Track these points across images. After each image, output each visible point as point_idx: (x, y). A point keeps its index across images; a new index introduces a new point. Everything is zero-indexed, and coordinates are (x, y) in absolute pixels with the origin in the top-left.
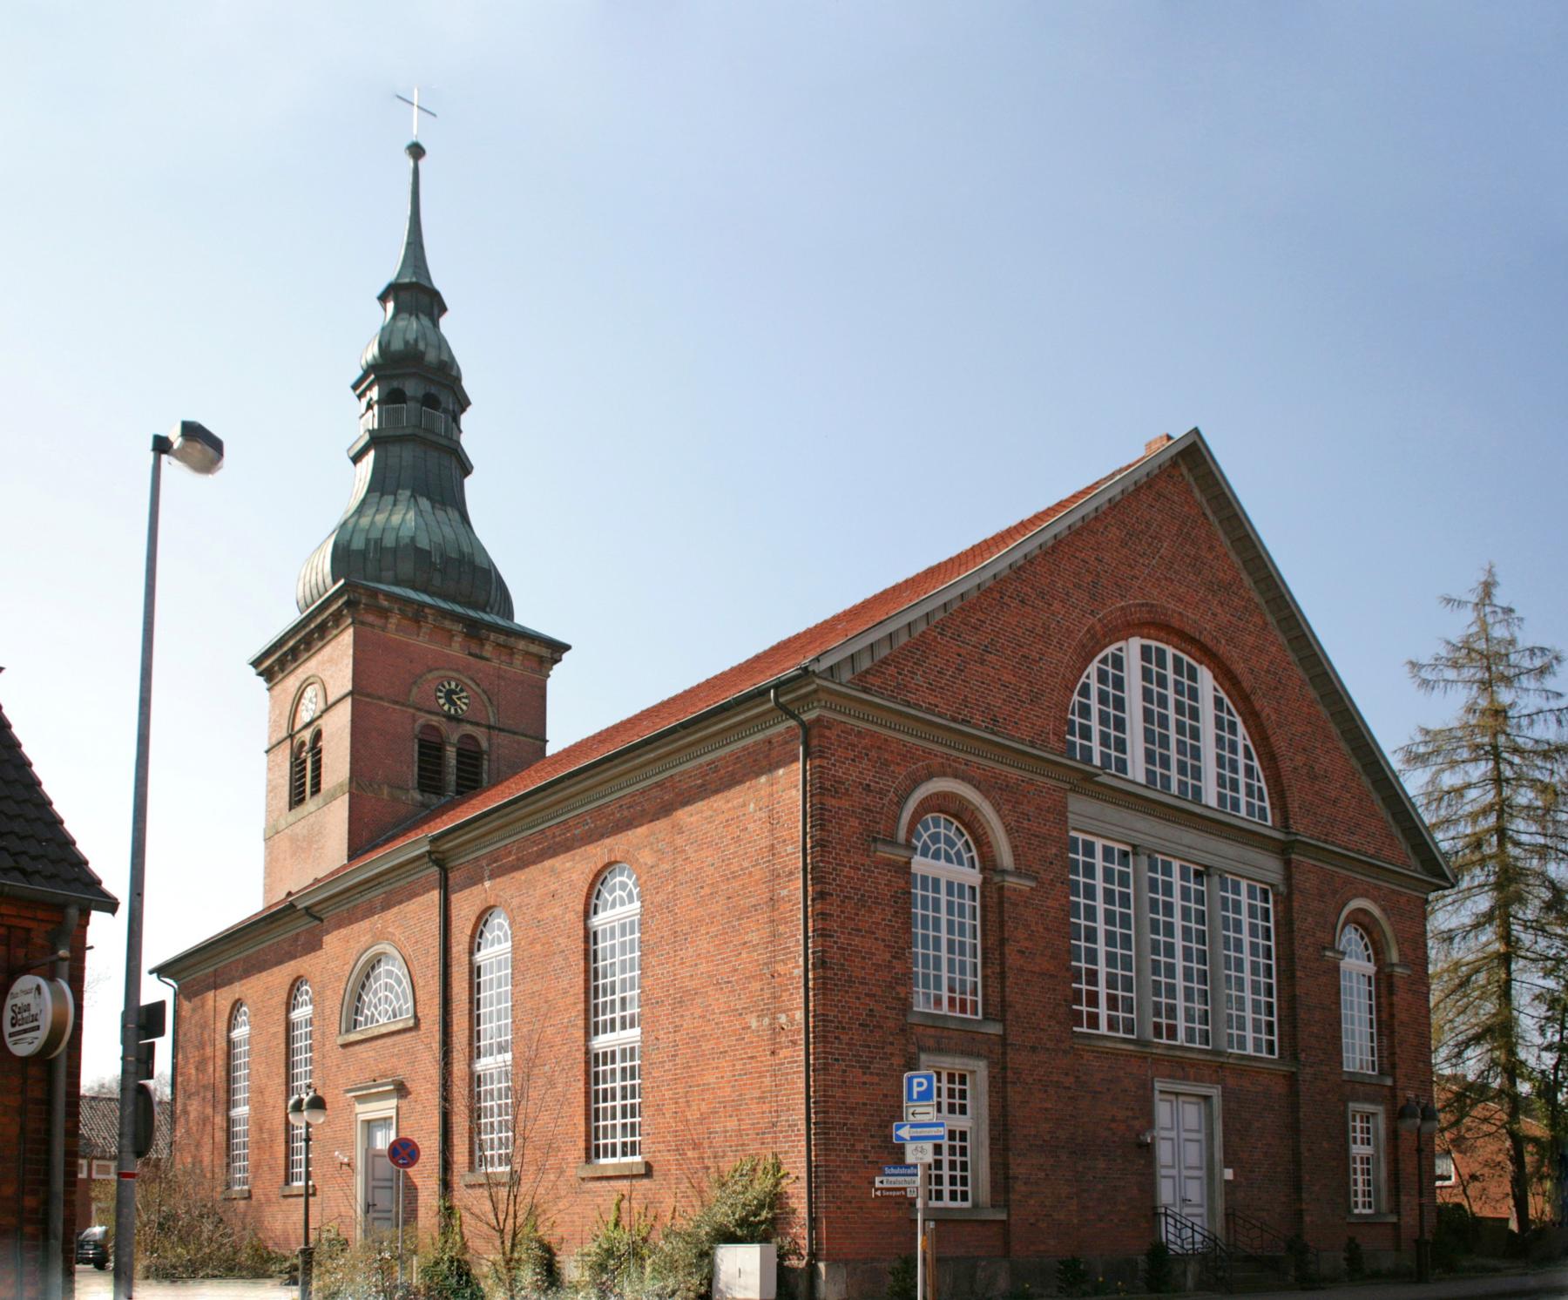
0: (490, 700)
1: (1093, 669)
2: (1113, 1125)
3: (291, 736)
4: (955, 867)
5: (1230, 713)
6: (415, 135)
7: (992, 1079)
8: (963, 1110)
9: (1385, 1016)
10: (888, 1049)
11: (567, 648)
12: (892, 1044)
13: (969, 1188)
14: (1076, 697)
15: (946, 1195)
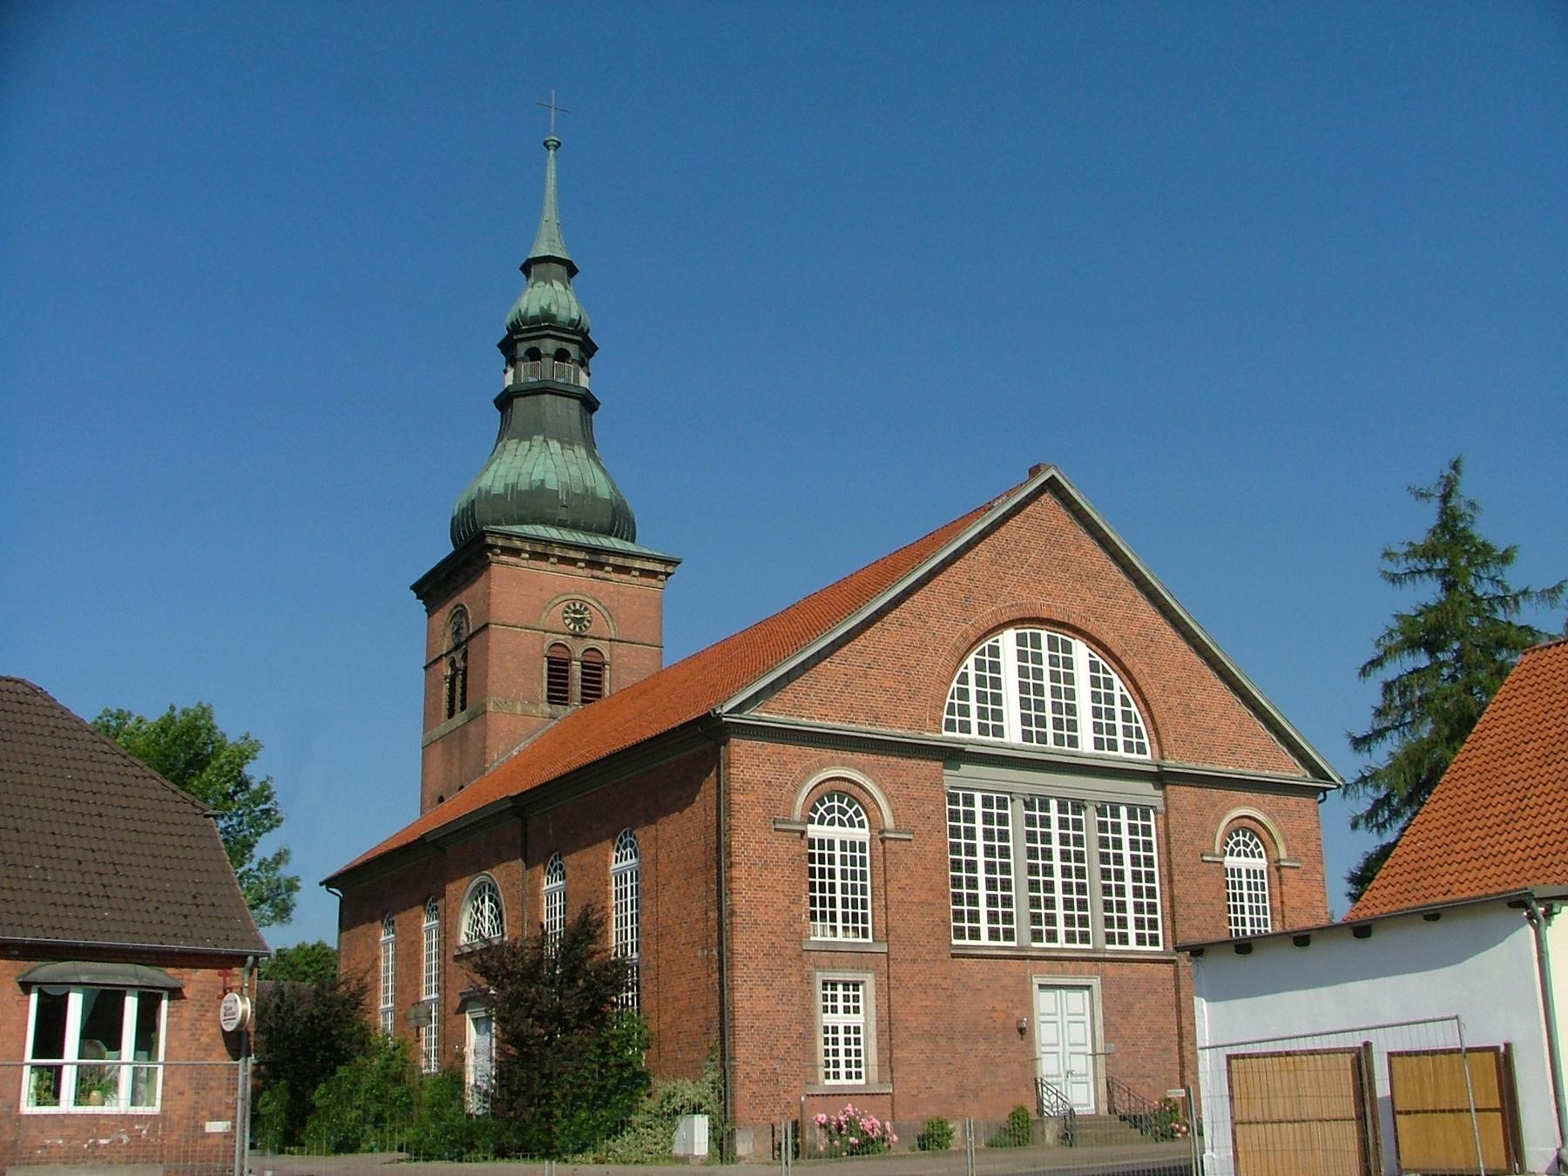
0: (610, 615)
1: (970, 661)
2: (994, 1015)
4: (848, 829)
5: (1105, 671)
7: (879, 986)
8: (856, 1010)
9: (1277, 904)
10: (787, 970)
12: (790, 966)
13: (863, 1069)
14: (955, 685)
15: (842, 1075)
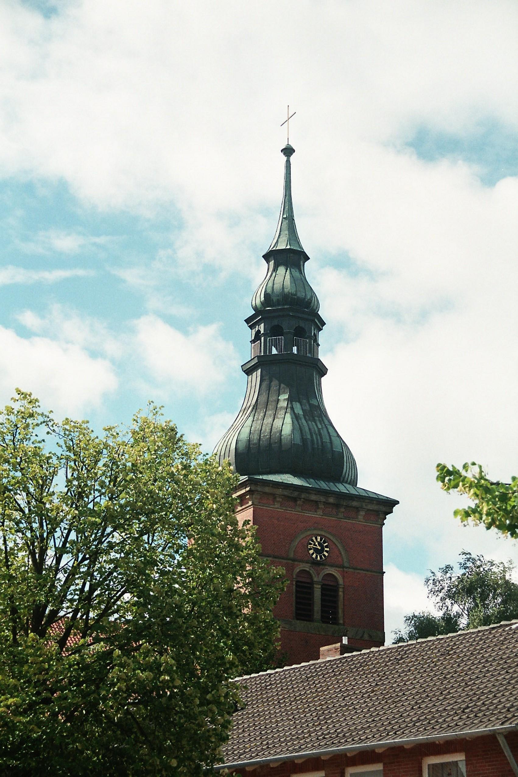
11: (397, 502)
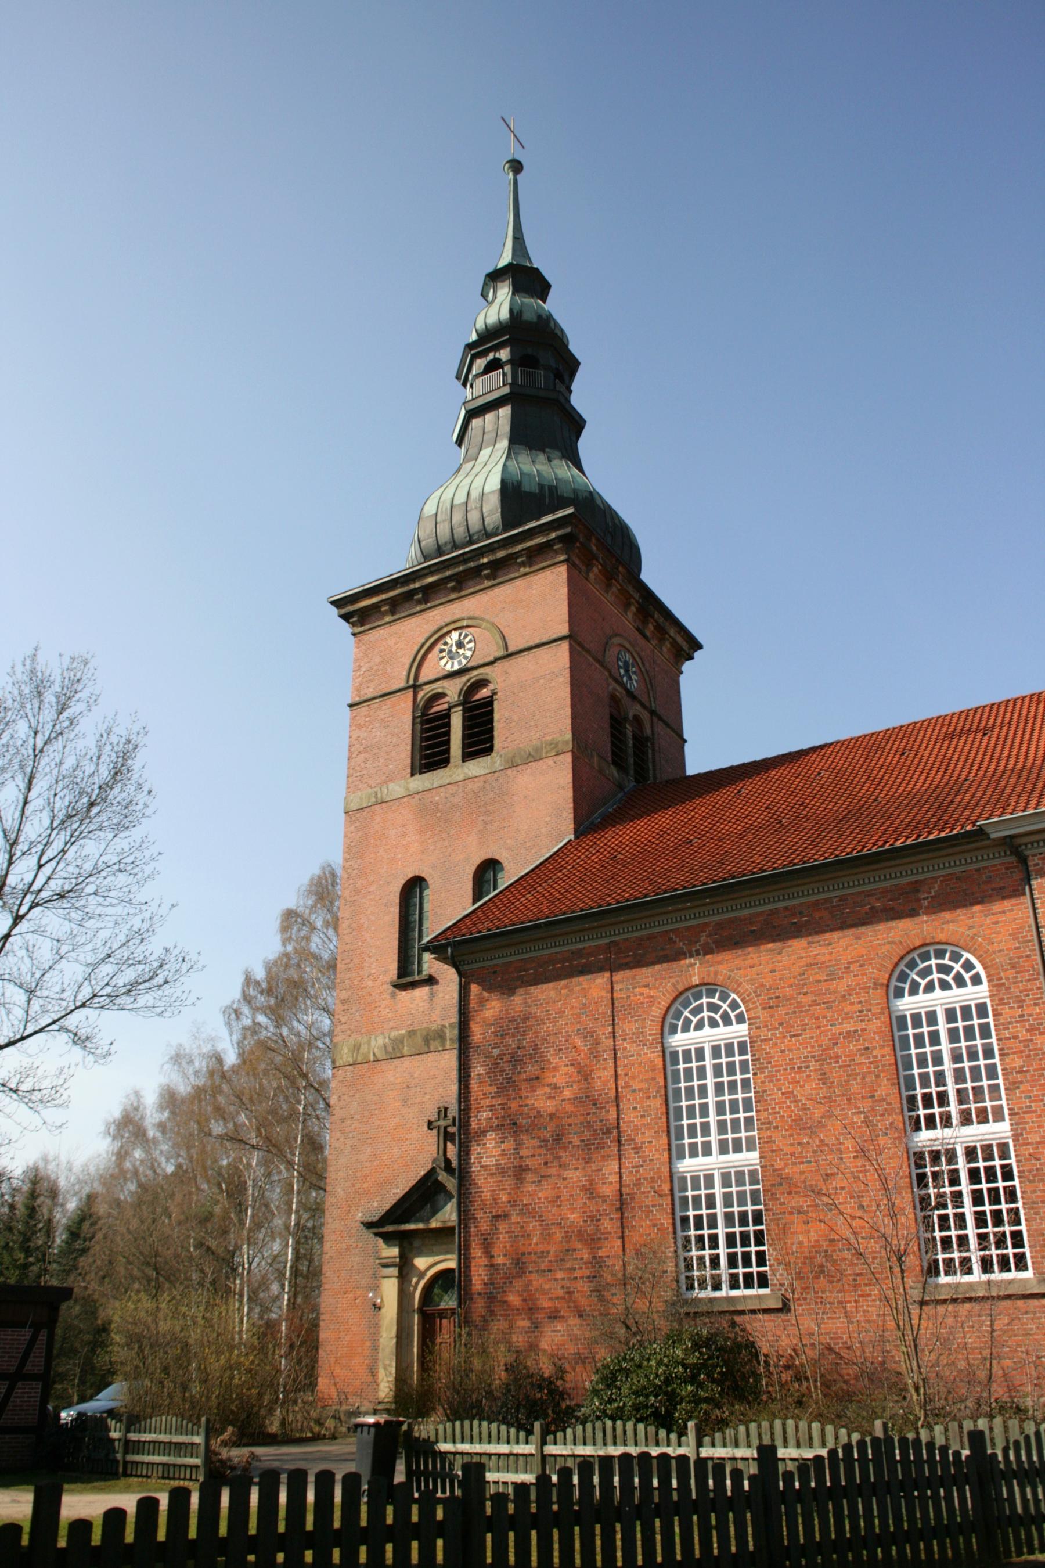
3: (416, 687)
6: (513, 151)
